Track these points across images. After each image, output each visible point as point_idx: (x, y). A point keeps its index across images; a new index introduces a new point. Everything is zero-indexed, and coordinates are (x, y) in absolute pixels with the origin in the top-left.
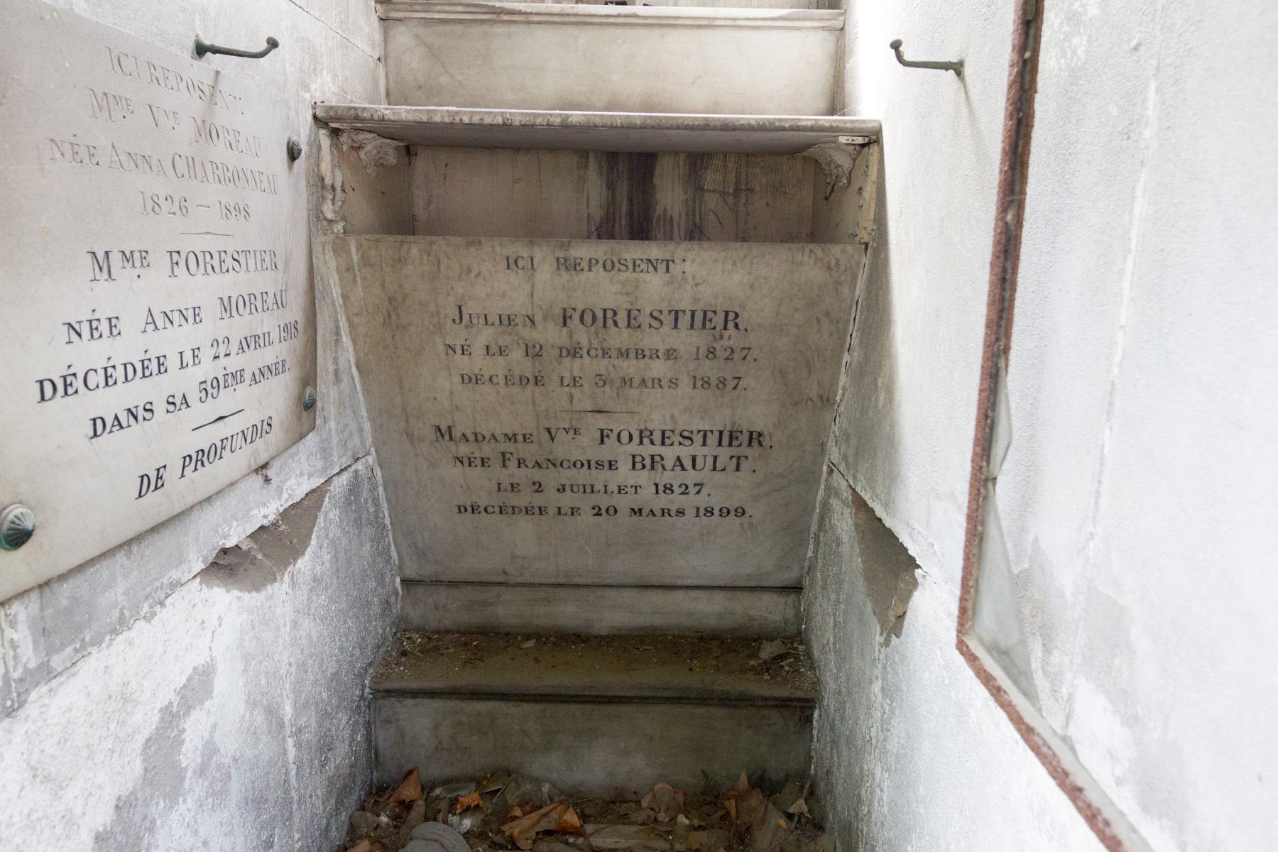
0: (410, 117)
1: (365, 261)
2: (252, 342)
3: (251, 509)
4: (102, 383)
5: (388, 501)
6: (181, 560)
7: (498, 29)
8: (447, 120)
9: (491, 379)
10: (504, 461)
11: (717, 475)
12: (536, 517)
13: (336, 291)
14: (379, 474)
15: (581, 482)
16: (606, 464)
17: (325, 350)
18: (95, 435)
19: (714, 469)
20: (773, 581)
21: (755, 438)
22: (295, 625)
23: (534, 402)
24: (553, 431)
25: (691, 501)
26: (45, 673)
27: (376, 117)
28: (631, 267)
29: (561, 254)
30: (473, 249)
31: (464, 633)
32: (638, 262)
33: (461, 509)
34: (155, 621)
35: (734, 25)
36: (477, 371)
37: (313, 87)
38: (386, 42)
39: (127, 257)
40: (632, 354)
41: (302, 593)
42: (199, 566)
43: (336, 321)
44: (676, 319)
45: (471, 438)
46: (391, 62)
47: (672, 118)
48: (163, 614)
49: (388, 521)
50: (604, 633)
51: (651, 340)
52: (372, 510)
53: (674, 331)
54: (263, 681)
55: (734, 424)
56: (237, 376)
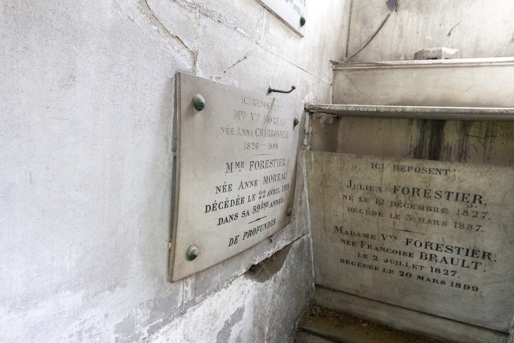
0: (340, 109)
1: (316, 161)
2: (273, 192)
3: (264, 251)
4: (224, 207)
5: (314, 252)
6: (239, 268)
7: (379, 72)
8: (354, 110)
9: (360, 211)
10: (362, 245)
11: (464, 269)
12: (373, 271)
13: (304, 171)
14: (312, 241)
15: (395, 259)
16: (408, 254)
17: (297, 193)
18: (219, 224)
19: (463, 266)
20: (492, 326)
21: (486, 255)
22: (273, 297)
23: (378, 223)
24: (385, 236)
25: (449, 278)
26: (193, 303)
28: (428, 171)
29: (396, 163)
30: (358, 159)
31: (337, 313)
32: (431, 170)
33: (342, 261)
34: (228, 289)
35: (491, 65)
36: (355, 207)
37: (306, 98)
38: (334, 78)
39: (237, 164)
40: (425, 209)
41: (277, 285)
42: (244, 271)
43: (303, 182)
44: (449, 196)
45: (349, 233)
46: (335, 85)
47: (454, 109)
48: (231, 287)
49: (312, 260)
50: (400, 329)
51: (434, 203)
52: (307, 255)
53: (447, 201)
54: (260, 317)
55: (475, 247)
56: (266, 204)
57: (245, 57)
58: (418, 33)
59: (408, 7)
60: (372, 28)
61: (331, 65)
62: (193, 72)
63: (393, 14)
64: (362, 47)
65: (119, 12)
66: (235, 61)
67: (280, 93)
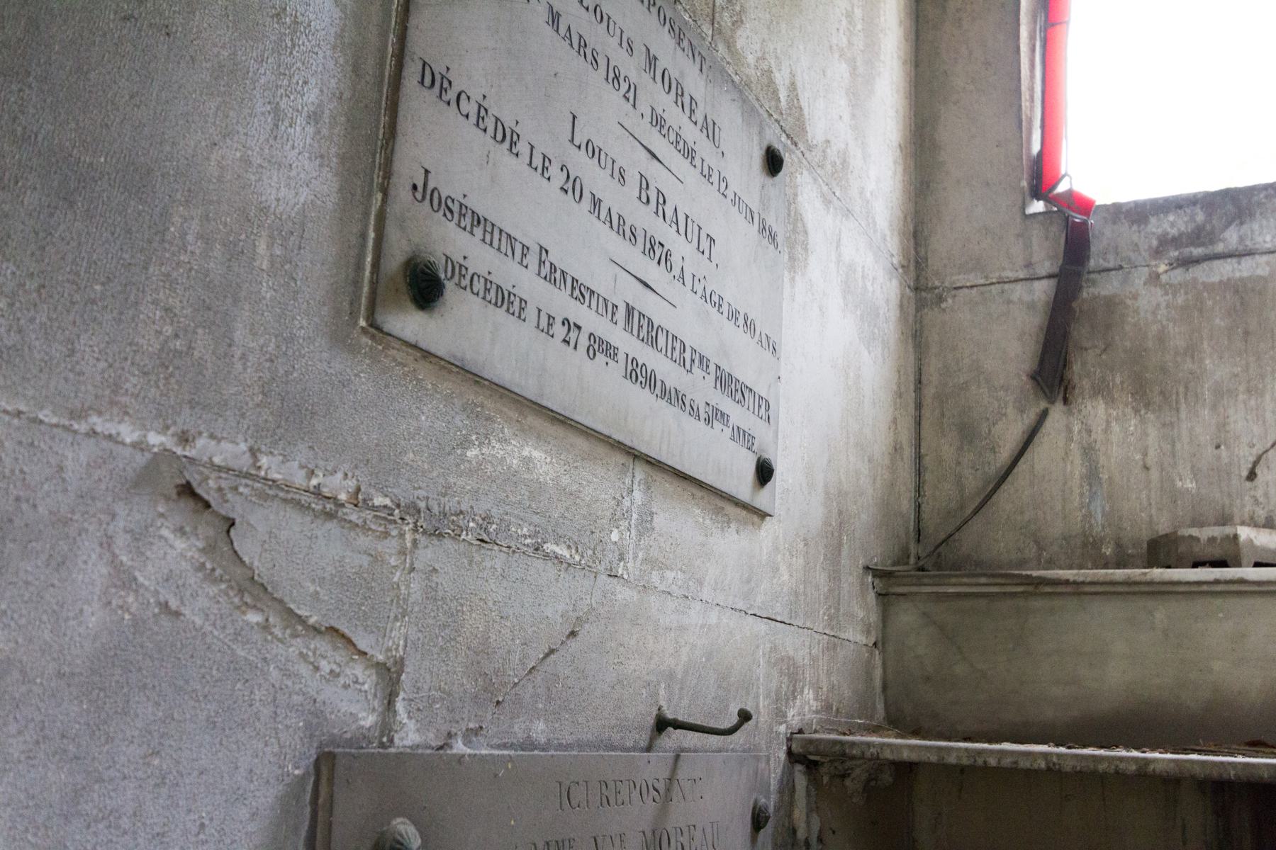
7: (1037, 603)
27: (868, 755)
37: (791, 713)
38: (884, 626)
57: (573, 634)
58: (1147, 468)
59: (1101, 390)
60: (993, 450)
61: (870, 579)
62: (382, 736)
63: (1057, 413)
64: (969, 511)
65: (131, 599)
66: (536, 654)
67: (697, 734)
